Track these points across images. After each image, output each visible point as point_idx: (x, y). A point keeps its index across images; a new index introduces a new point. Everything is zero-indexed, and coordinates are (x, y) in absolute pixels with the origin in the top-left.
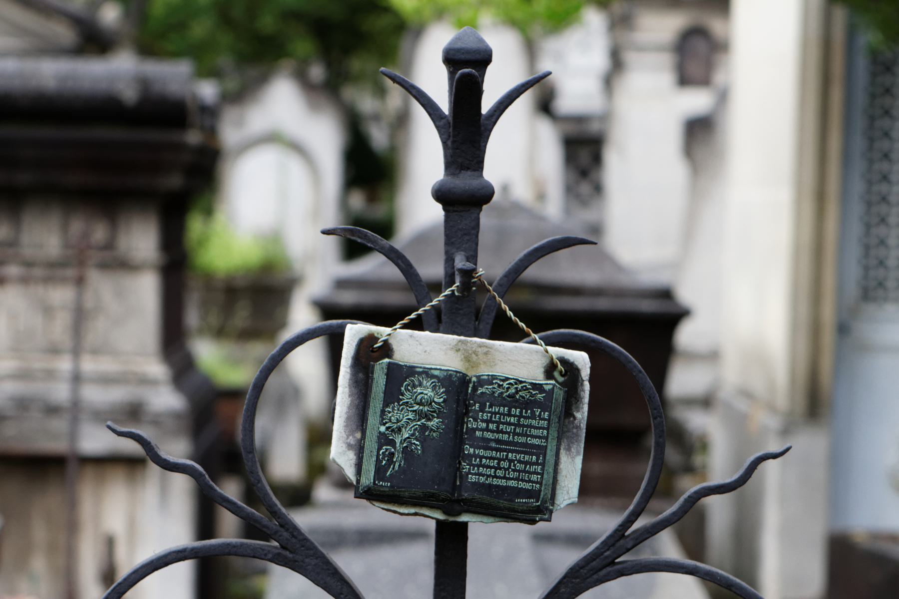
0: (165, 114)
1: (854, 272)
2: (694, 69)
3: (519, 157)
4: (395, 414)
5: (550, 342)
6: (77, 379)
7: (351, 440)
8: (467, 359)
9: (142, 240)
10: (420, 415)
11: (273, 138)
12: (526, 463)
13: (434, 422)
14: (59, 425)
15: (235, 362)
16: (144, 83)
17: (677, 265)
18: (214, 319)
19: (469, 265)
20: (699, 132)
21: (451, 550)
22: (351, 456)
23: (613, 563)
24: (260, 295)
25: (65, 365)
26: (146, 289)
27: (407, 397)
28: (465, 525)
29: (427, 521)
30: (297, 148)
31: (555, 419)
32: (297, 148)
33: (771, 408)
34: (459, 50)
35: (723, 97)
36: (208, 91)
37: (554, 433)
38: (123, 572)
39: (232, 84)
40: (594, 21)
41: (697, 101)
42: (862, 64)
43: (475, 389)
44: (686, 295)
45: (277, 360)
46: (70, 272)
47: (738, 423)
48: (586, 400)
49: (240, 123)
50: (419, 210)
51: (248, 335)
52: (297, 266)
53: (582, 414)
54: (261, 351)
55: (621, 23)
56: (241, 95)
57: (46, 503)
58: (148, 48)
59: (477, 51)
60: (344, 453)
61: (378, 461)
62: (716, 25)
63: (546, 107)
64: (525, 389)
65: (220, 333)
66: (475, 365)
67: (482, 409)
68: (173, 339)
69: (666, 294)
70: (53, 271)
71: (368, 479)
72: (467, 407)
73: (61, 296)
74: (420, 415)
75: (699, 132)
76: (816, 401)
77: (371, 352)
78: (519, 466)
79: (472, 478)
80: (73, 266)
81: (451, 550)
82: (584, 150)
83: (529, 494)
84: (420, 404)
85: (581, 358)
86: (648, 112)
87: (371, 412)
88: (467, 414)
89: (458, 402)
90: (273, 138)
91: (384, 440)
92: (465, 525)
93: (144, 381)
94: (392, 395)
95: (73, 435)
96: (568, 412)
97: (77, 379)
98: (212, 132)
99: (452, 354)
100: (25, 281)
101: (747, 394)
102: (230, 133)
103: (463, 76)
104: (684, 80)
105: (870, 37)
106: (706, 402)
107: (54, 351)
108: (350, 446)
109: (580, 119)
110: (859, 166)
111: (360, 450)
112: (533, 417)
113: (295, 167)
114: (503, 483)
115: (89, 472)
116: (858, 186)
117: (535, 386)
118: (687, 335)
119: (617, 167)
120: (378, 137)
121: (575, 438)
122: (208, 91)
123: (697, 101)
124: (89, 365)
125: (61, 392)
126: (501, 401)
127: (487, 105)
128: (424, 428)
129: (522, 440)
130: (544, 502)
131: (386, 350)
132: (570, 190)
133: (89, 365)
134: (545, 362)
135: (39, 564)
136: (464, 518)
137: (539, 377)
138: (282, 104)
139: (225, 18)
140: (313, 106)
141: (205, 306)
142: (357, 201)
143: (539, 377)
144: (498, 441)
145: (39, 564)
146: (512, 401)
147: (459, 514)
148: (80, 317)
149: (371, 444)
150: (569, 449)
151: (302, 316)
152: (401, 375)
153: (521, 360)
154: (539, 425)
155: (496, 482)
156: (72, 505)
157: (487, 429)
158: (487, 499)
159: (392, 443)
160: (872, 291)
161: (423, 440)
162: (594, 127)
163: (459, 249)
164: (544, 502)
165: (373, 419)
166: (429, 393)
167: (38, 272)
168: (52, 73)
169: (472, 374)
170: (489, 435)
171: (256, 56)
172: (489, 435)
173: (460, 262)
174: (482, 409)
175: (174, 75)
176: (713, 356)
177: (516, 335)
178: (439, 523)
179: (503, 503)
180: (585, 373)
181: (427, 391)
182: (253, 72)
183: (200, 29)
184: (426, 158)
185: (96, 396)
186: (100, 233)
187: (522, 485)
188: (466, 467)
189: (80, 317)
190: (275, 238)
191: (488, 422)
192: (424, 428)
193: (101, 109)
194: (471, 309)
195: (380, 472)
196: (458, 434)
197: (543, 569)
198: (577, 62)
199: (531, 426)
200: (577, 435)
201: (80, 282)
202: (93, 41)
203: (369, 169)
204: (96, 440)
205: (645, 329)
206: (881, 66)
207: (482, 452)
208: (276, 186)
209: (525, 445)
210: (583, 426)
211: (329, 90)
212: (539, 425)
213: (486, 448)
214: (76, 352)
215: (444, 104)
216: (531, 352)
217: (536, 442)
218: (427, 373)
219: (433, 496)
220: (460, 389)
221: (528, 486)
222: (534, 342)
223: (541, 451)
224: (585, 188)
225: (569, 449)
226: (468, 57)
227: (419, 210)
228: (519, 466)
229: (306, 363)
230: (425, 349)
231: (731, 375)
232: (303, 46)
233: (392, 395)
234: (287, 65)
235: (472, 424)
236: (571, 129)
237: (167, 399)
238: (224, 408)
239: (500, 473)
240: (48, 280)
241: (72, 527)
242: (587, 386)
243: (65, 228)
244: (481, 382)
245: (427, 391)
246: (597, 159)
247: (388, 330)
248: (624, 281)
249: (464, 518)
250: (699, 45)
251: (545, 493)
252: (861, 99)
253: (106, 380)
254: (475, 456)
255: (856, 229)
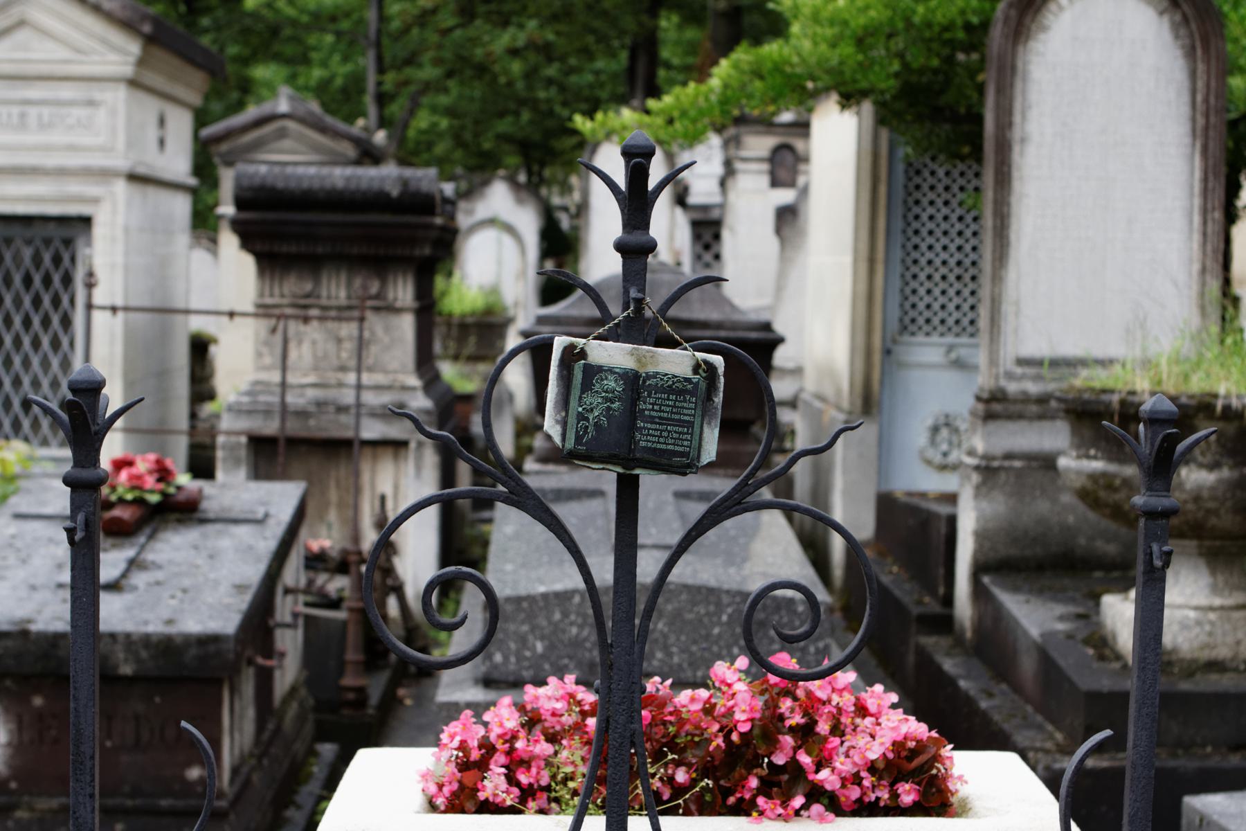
0: (420, 204)
1: (895, 313)
2: (783, 174)
3: (668, 228)
4: (589, 399)
5: (697, 349)
6: (359, 387)
7: (559, 417)
8: (639, 361)
9: (403, 292)
10: (606, 400)
11: (492, 222)
12: (680, 433)
13: (616, 405)
14: (344, 418)
15: (468, 377)
16: (405, 183)
17: (771, 308)
18: (452, 345)
19: (640, 295)
20: (787, 217)
21: (628, 492)
22: (558, 428)
23: (740, 503)
24: (485, 329)
25: (351, 378)
26: (406, 325)
27: (597, 387)
28: (637, 476)
29: (607, 479)
30: (509, 229)
31: (700, 403)
32: (509, 229)
33: (839, 408)
34: (632, 146)
35: (805, 192)
36: (448, 188)
37: (699, 412)
38: (391, 517)
39: (464, 185)
40: (715, 140)
41: (786, 196)
42: (900, 168)
43: (644, 381)
44: (779, 328)
45: (495, 379)
46: (356, 313)
47: (815, 417)
48: (722, 389)
49: (470, 212)
50: (601, 262)
51: (475, 358)
52: (511, 313)
53: (719, 399)
54: (485, 368)
55: (731, 143)
56: (470, 193)
57: (341, 471)
58: (403, 162)
59: (646, 147)
60: (552, 427)
61: (577, 432)
62: (799, 145)
63: (681, 199)
64: (679, 381)
65: (456, 358)
66: (644, 365)
67: (649, 396)
68: (425, 361)
69: (767, 327)
70: (342, 313)
71: (570, 444)
72: (639, 394)
73: (348, 330)
74: (606, 400)
75: (787, 217)
76: (870, 401)
77: (572, 355)
78: (675, 435)
79: (643, 444)
80: (355, 311)
81: (628, 492)
82: (707, 230)
83: (682, 454)
84: (606, 392)
85: (718, 360)
86: (752, 203)
87: (572, 398)
88: (638, 399)
89: (632, 390)
90: (492, 222)
91: (581, 417)
92: (637, 476)
93: (405, 388)
94: (587, 386)
95: (357, 427)
96: (709, 397)
97: (359, 387)
98: (452, 217)
99: (629, 357)
100: (322, 319)
101: (821, 398)
102: (463, 221)
103: (636, 164)
104: (775, 183)
105: (905, 150)
106: (793, 404)
107: (343, 369)
108: (557, 422)
109: (705, 208)
110: (899, 239)
111: (564, 424)
112: (685, 401)
113: (507, 240)
114: (663, 447)
115: (368, 451)
116: (898, 253)
117: (686, 380)
118: (781, 356)
119: (729, 243)
120: (565, 222)
121: (713, 416)
122: (448, 188)
123: (786, 196)
124: (366, 378)
125: (348, 397)
126: (662, 390)
127: (651, 185)
128: (609, 408)
129: (677, 417)
130: (693, 460)
131: (583, 354)
132: (697, 258)
133: (366, 378)
134: (693, 363)
135: (333, 515)
136: (637, 471)
137: (688, 373)
138: (499, 199)
139: (459, 141)
140: (520, 201)
141: (446, 338)
142: (549, 265)
143: (688, 373)
144: (660, 418)
145: (333, 515)
146: (670, 390)
147: (633, 469)
148: (361, 344)
149: (572, 420)
150: (709, 423)
151: (513, 340)
152: (593, 372)
153: (676, 362)
154: (689, 408)
155: (659, 446)
156: (357, 475)
157: (653, 410)
158: (652, 458)
159: (587, 419)
160: (907, 326)
161: (609, 417)
162: (715, 214)
163: (633, 285)
164: (693, 460)
165: (573, 403)
166: (613, 384)
167: (333, 313)
168: (340, 176)
169: (642, 371)
170: (654, 414)
171: (480, 169)
172: (654, 414)
173: (633, 293)
174: (649, 396)
175: (425, 177)
176: (798, 372)
177: (672, 344)
178: (619, 474)
179: (664, 461)
180: (721, 370)
181: (611, 383)
182: (477, 178)
183: (440, 149)
184: (605, 222)
185: (371, 399)
186: (374, 288)
187: (677, 448)
188: (638, 436)
189: (361, 344)
190: (494, 290)
191: (653, 404)
192: (609, 408)
193: (375, 201)
194: (638, 328)
195: (578, 439)
196: (632, 414)
197: (683, 517)
198: (704, 168)
199: (683, 408)
200: (716, 414)
201: (362, 320)
202: (369, 155)
203: (559, 244)
204: (372, 430)
205: (755, 348)
206: (913, 171)
207: (649, 426)
208: (494, 258)
209: (679, 420)
210: (720, 407)
211: (530, 188)
212: (689, 408)
213: (652, 423)
214: (359, 371)
215: (621, 180)
216: (683, 356)
217: (687, 418)
218: (611, 370)
219: (615, 456)
220: (634, 382)
221: (681, 449)
222: (686, 349)
223: (690, 424)
224: (708, 257)
225: (709, 423)
226: (638, 151)
227: (601, 262)
228: (675, 435)
229: (517, 377)
230: (611, 354)
231: (810, 384)
232: (513, 160)
233: (587, 386)
234: (501, 172)
235: (642, 406)
236: (698, 216)
237: (420, 402)
238: (460, 408)
239: (662, 440)
240: (339, 319)
241: (357, 490)
242: (722, 379)
243: (349, 285)
244: (648, 377)
245: (611, 383)
246: (717, 237)
247: (584, 341)
248: (736, 317)
249: (637, 471)
250: (788, 157)
251: (693, 454)
252: (900, 193)
253: (378, 388)
254: (645, 428)
255: (897, 283)
